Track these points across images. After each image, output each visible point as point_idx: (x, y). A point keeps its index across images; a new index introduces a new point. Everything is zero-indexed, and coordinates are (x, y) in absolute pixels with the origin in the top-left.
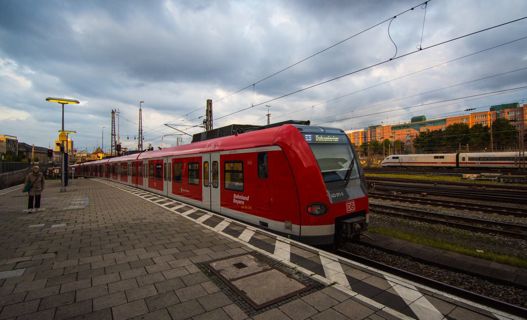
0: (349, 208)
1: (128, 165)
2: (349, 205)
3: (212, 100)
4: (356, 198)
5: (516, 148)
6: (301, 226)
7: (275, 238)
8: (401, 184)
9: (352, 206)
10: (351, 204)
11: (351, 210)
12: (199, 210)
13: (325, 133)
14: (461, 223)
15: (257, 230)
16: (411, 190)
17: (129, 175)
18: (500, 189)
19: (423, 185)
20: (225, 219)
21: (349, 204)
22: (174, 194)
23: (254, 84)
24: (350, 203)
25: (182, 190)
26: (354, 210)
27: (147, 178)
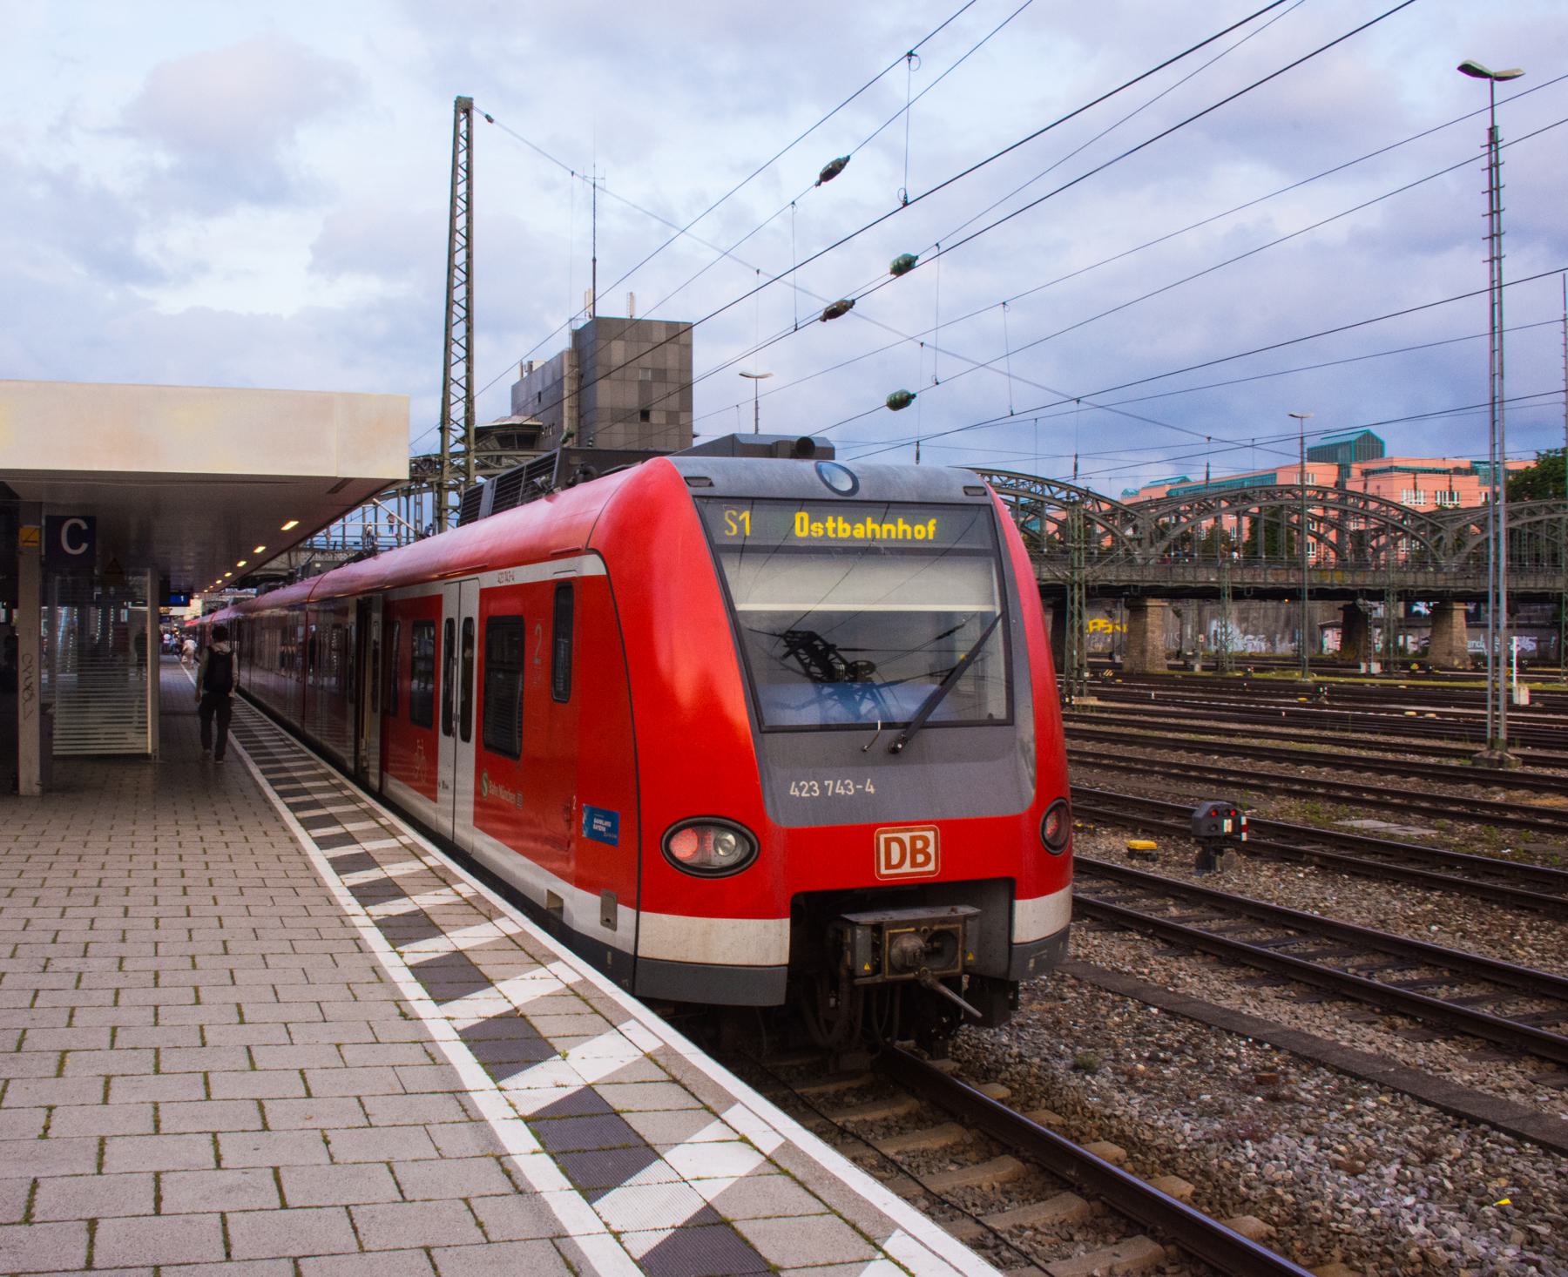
0: (895, 859)
1: (450, 622)
2: (895, 847)
3: (679, 334)
4: (954, 814)
5: (1087, 581)
6: (643, 915)
7: (875, 1232)
8: (1550, 755)
9: (914, 852)
10: (913, 840)
11: (907, 868)
12: (415, 844)
13: (857, 497)
14: (1299, 949)
15: (788, 1146)
16: (457, 698)
17: (456, 725)
18: (1353, 752)
19: (1193, 737)
20: (732, 1101)
21: (901, 842)
22: (514, 848)
23: (906, 204)
24: (906, 837)
25: (849, 940)
26: (930, 873)
27: (466, 738)
